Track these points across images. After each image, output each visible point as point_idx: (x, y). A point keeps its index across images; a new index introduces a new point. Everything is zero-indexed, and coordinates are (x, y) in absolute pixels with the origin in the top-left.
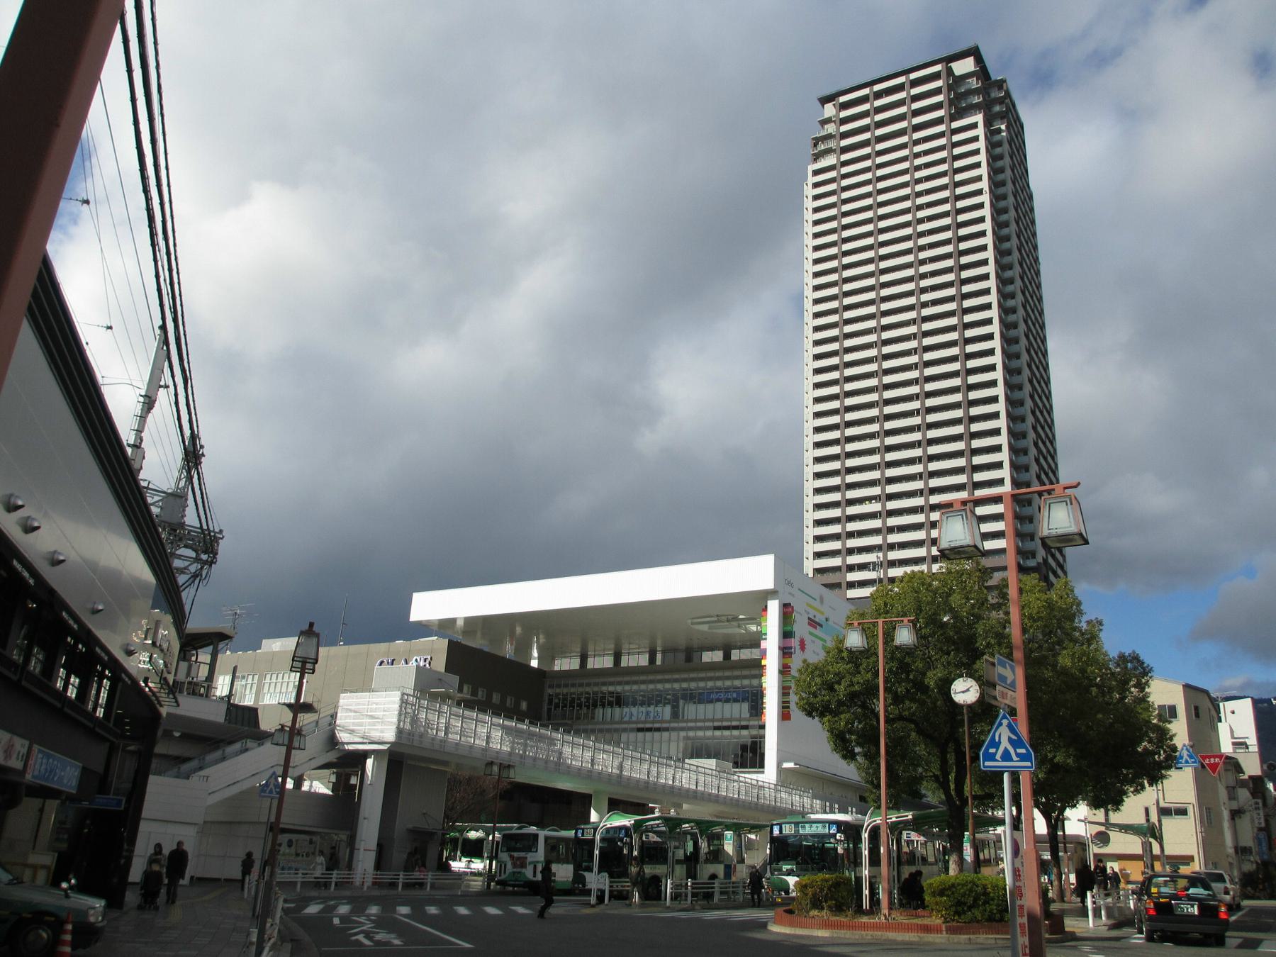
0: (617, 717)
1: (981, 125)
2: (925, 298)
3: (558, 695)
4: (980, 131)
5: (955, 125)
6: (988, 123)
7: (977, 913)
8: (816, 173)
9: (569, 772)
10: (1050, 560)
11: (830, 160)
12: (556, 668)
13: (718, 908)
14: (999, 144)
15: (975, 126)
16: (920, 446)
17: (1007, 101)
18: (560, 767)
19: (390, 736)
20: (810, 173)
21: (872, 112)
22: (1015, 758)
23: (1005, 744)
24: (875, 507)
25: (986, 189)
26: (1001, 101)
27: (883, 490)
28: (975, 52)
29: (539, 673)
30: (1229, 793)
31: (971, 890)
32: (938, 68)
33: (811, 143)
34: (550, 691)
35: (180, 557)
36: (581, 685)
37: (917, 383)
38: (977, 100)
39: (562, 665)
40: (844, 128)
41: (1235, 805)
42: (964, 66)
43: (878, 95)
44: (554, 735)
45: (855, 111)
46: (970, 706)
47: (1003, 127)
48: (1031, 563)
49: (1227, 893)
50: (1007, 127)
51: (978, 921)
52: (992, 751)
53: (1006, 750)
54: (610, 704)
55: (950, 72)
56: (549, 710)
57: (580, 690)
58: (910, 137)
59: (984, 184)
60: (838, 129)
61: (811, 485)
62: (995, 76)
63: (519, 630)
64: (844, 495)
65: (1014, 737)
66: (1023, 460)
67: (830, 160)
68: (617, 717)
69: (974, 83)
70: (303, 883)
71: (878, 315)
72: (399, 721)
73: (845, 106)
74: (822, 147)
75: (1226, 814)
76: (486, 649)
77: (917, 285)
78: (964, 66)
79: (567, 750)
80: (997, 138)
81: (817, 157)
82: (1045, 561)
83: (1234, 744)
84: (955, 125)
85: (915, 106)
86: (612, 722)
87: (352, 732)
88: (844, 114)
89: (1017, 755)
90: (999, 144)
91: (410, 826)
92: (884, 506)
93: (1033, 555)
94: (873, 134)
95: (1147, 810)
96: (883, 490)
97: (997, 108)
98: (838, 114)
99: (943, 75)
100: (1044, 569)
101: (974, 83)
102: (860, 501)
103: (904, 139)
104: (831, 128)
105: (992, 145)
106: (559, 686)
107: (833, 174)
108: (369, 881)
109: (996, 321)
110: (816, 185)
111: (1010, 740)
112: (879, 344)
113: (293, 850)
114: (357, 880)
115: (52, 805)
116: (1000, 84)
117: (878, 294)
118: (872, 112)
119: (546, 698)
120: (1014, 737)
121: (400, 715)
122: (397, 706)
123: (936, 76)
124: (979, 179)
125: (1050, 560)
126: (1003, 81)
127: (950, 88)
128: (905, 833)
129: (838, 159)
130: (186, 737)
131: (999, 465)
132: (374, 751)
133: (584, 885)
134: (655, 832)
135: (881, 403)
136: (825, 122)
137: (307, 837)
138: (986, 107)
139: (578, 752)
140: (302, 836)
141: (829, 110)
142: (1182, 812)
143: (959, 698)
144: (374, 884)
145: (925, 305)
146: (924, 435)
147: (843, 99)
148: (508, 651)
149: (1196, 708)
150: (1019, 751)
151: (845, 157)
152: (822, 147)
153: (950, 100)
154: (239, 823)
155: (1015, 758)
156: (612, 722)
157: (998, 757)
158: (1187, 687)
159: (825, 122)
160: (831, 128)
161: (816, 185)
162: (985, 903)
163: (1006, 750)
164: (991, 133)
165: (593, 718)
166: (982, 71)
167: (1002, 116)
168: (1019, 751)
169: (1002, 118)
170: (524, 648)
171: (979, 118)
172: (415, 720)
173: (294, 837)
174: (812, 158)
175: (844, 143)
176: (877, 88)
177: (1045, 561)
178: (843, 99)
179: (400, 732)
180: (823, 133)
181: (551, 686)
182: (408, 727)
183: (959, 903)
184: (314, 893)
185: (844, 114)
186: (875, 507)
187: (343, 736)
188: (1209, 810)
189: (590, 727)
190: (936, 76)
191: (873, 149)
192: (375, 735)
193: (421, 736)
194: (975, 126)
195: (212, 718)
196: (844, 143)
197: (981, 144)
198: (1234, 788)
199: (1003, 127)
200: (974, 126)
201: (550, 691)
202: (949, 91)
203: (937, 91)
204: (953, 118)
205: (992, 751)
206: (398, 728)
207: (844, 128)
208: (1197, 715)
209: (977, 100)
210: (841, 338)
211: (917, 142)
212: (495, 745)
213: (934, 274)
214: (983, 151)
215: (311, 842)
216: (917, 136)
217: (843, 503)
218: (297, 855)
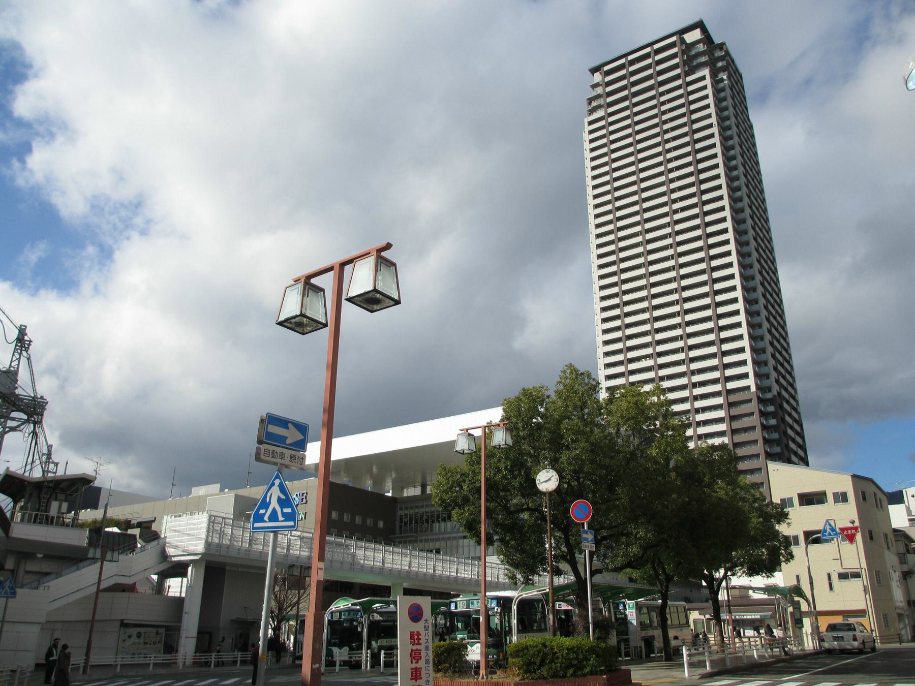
0: (449, 529)
1: (708, 77)
2: (675, 206)
3: (406, 515)
4: (708, 82)
5: (689, 79)
6: (714, 75)
7: (544, 671)
8: (590, 123)
9: (363, 568)
10: (784, 393)
11: (600, 113)
12: (405, 495)
13: (382, 674)
14: (723, 90)
15: (703, 78)
16: (679, 315)
17: (728, 58)
18: (353, 564)
19: (200, 547)
20: (586, 124)
21: (628, 76)
22: (281, 518)
23: (274, 504)
24: (649, 363)
25: (715, 123)
26: (722, 59)
27: (654, 350)
28: (700, 25)
29: (393, 499)
30: (900, 559)
31: (539, 651)
32: (674, 39)
33: (585, 102)
34: (400, 512)
35: (14, 419)
36: (422, 507)
37: (674, 269)
38: (703, 59)
39: (409, 492)
40: (608, 89)
41: (905, 568)
42: (693, 36)
43: (632, 63)
44: (348, 542)
45: (622, 81)
46: (550, 493)
47: (725, 77)
48: (769, 396)
49: (855, 639)
50: (729, 77)
51: (545, 678)
52: (262, 511)
53: (274, 510)
54: (444, 520)
55: (683, 41)
56: (401, 527)
57: (422, 510)
58: (657, 91)
59: (713, 120)
60: (604, 90)
61: (602, 349)
62: (717, 40)
63: (375, 469)
64: (625, 356)
65: (283, 497)
66: (757, 320)
67: (600, 113)
68: (449, 529)
69: (701, 47)
70: (154, 664)
71: (642, 222)
72: (207, 536)
73: (608, 73)
74: (594, 104)
75: (896, 576)
76: (350, 484)
77: (669, 197)
78: (690, 37)
79: (360, 553)
80: (721, 85)
81: (591, 112)
82: (779, 394)
83: (910, 520)
84: (689, 79)
85: (659, 68)
86: (446, 532)
87: (176, 547)
88: (608, 79)
89: (283, 514)
90: (723, 90)
91: (234, 617)
92: (655, 362)
93: (769, 389)
94: (630, 91)
95: (829, 576)
96: (654, 350)
97: (720, 64)
98: (603, 79)
99: (678, 43)
100: (778, 400)
101: (701, 47)
102: (638, 359)
103: (653, 93)
104: (599, 90)
105: (717, 91)
106: (406, 508)
107: (602, 123)
108: (189, 661)
109: (729, 219)
110: (591, 132)
111: (280, 500)
112: (644, 243)
113: (141, 640)
114: (180, 661)
115: (676, 622)
116: (721, 46)
117: (641, 207)
118: (628, 76)
119: (398, 519)
120: (283, 497)
121: (208, 532)
122: (205, 525)
123: (673, 45)
124: (709, 116)
125: (784, 393)
126: (723, 44)
127: (683, 52)
128: (557, 604)
129: (606, 111)
130: (47, 557)
131: (738, 325)
132: (192, 561)
133: (332, 658)
134: (378, 613)
135: (649, 286)
136: (594, 86)
137: (154, 630)
138: (711, 64)
139: (370, 554)
140: (151, 629)
141: (598, 77)
142: (857, 575)
143: (542, 487)
144: (194, 663)
145: (676, 212)
146: (682, 307)
147: (606, 68)
148: (368, 485)
149: (863, 494)
150: (285, 510)
151: (610, 110)
152: (594, 104)
153: (684, 61)
154: (110, 620)
155: (281, 518)
156: (446, 532)
157: (266, 518)
158: (855, 477)
159: (594, 86)
160: (599, 90)
161: (591, 132)
162: (552, 661)
163: (274, 510)
164: (716, 82)
165: (432, 530)
166: (707, 38)
167: (723, 69)
168: (285, 510)
169: (724, 71)
170: (379, 480)
171: (706, 72)
172: (222, 534)
173: (142, 630)
174: (586, 113)
175: (609, 99)
176: (630, 58)
177: (779, 394)
178: (606, 68)
179: (208, 545)
180: (594, 94)
181: (401, 509)
182: (216, 540)
183: (530, 663)
184: (163, 671)
185: (608, 79)
186: (649, 363)
187: (170, 551)
188: (877, 573)
189: (430, 537)
190: (673, 45)
191: (631, 102)
192: (192, 548)
193: (228, 547)
194: (703, 78)
195: (81, 544)
196: (609, 99)
197: (709, 91)
198: (904, 554)
199: (725, 77)
200: (703, 78)
201: (400, 512)
202: (683, 55)
203: (674, 56)
204: (687, 74)
205: (262, 511)
206: (206, 542)
207: (608, 89)
208: (864, 499)
209: (703, 59)
210: (616, 241)
211: (662, 94)
212: (295, 552)
213: (681, 188)
214: (711, 96)
215: (157, 633)
216: (661, 89)
217: (626, 362)
218: (146, 643)
